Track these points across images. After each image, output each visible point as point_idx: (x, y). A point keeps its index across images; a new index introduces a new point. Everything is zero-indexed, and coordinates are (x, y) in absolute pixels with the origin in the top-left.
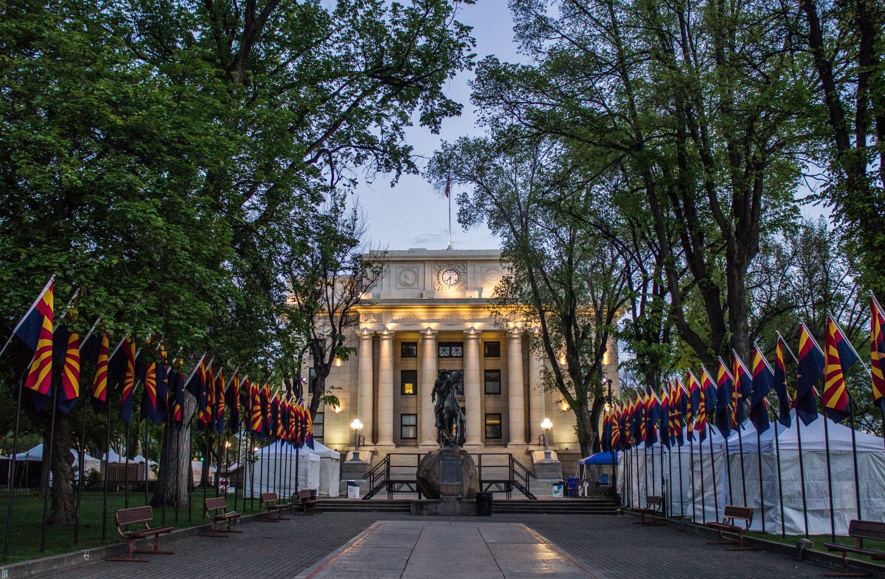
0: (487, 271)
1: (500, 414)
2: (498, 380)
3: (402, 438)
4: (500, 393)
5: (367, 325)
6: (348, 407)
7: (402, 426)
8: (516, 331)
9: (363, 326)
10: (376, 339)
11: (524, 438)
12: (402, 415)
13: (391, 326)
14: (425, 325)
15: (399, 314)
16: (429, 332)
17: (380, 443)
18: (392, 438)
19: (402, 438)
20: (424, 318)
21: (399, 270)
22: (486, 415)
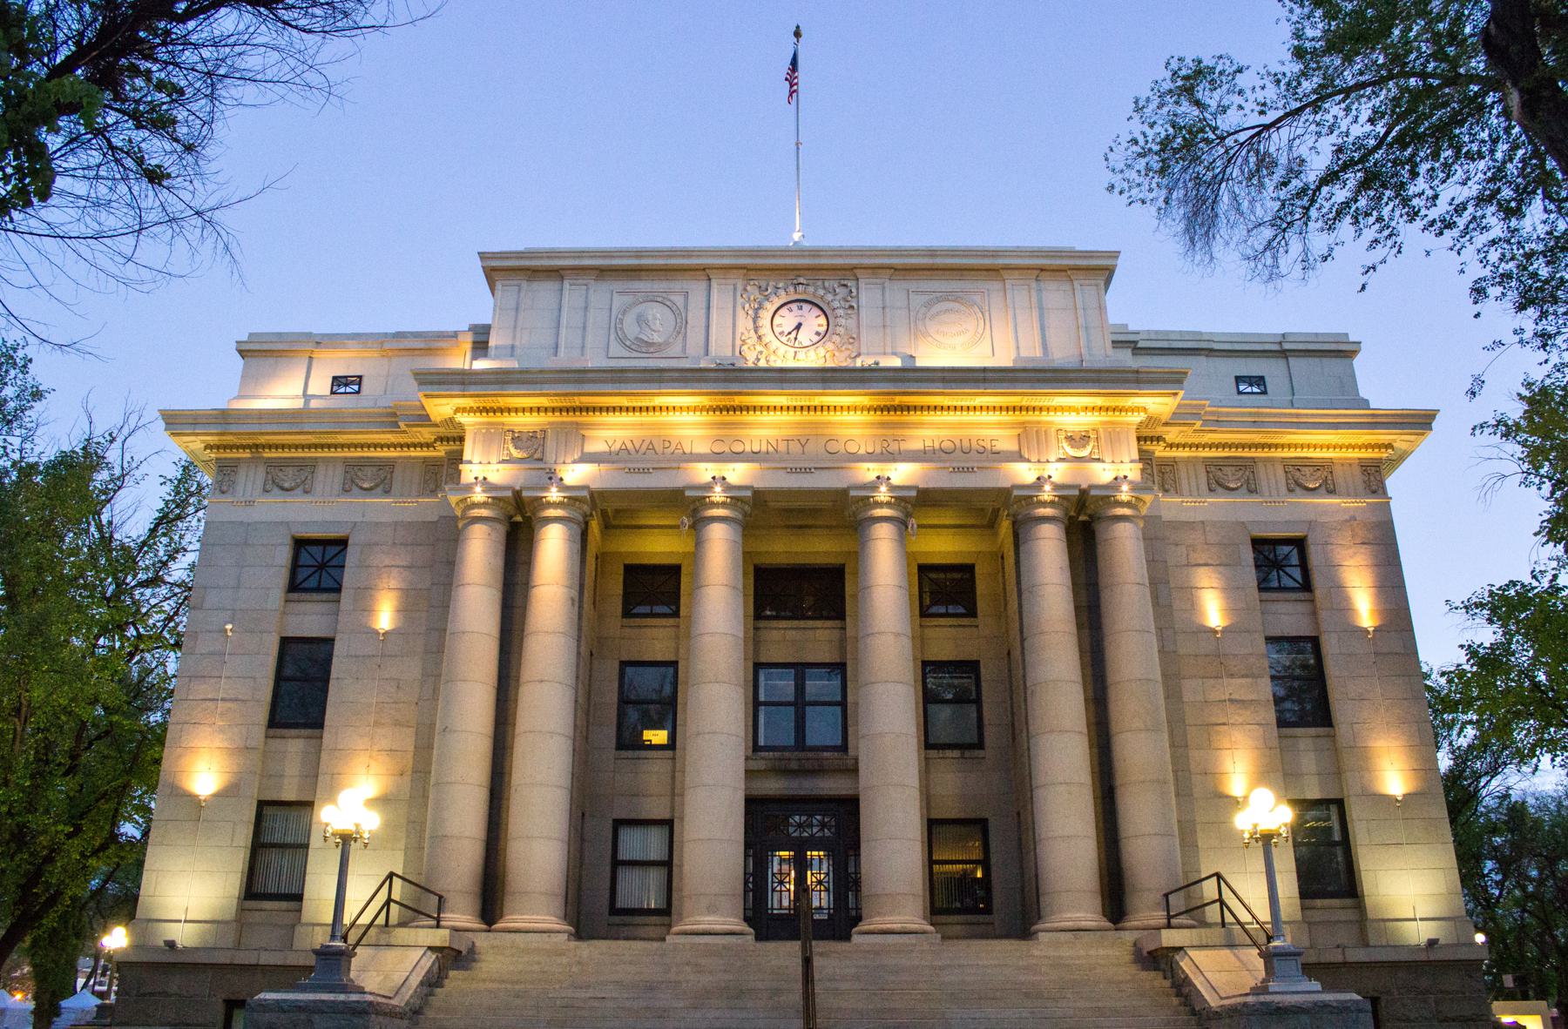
0: (929, 305)
1: (981, 825)
2: (970, 698)
3: (614, 910)
4: (980, 745)
5: (486, 468)
6: (407, 779)
7: (616, 863)
8: (1047, 494)
9: (469, 473)
10: (518, 526)
11: (1096, 902)
12: (619, 824)
13: (576, 474)
14: (704, 472)
15: (612, 431)
16: (718, 494)
17: (512, 920)
18: (558, 904)
19: (614, 910)
20: (702, 448)
21: (619, 301)
22: (925, 664)
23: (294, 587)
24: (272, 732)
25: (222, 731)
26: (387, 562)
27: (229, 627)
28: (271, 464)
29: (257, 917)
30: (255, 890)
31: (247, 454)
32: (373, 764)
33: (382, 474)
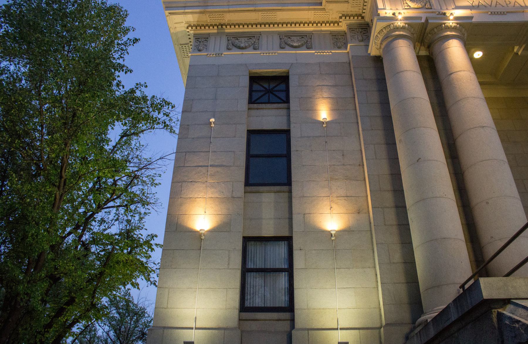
23: (251, 101)
24: (249, 189)
25: (212, 186)
26: (318, 84)
27: (212, 120)
28: (229, 36)
29: (254, 326)
30: (247, 304)
31: (215, 31)
32: (334, 206)
33: (304, 40)
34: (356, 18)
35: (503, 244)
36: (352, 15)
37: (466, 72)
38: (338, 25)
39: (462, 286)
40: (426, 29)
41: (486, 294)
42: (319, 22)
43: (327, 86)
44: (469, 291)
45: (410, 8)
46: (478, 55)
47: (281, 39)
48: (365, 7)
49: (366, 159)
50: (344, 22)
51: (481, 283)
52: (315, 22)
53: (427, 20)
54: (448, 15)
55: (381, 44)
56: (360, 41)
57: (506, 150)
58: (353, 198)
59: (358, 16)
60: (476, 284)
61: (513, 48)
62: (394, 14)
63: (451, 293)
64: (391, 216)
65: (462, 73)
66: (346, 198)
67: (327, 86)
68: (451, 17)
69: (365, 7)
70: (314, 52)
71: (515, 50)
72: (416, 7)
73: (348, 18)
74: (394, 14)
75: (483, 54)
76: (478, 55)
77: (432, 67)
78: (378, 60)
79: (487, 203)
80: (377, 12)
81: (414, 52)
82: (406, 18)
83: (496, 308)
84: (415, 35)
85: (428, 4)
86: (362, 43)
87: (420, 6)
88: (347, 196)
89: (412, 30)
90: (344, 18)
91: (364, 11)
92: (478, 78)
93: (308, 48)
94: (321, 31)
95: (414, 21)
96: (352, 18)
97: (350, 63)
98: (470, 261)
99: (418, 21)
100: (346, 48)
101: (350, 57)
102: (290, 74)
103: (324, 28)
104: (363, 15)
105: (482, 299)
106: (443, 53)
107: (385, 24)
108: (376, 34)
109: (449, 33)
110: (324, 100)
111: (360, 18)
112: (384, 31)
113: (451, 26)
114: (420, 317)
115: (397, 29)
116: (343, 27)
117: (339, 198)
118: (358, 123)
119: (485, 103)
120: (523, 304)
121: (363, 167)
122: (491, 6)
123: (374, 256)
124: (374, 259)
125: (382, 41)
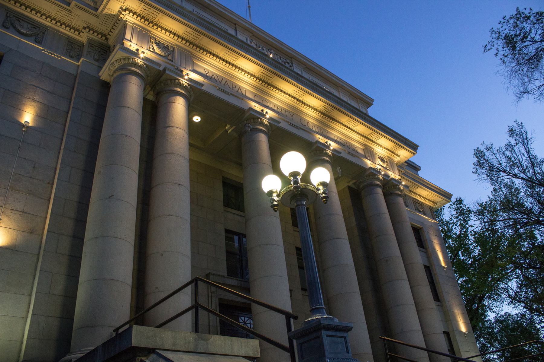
34: (100, 36)
35: (163, 296)
36: (97, 31)
37: (181, 130)
38: (79, 34)
39: (116, 330)
40: (161, 77)
41: (135, 342)
42: (59, 21)
43: (43, 89)
44: (121, 335)
45: (154, 52)
46: (197, 119)
47: (7, 17)
48: (112, 30)
49: (58, 179)
50: (86, 34)
51: (133, 330)
52: (55, 19)
53: (164, 70)
54: (184, 73)
55: (114, 72)
56: (95, 60)
57: (192, 210)
58: (30, 216)
59: (103, 35)
60: (130, 330)
61: (226, 126)
62: (137, 50)
63: (104, 334)
64: (65, 244)
65: (177, 130)
66: (21, 213)
67: (43, 89)
68: (186, 77)
69: (112, 30)
70: (42, 48)
71: (227, 128)
72: (160, 53)
73: (91, 32)
74: (137, 50)
75: (193, 117)
76: (197, 119)
77: (154, 114)
78: (106, 86)
79: (162, 255)
80: (123, 40)
81: (142, 93)
82: (146, 59)
83: (140, 356)
84: (149, 78)
85: (171, 56)
86: (97, 64)
87: (163, 54)
88: (23, 212)
89: (149, 72)
90: (87, 30)
91: (110, 33)
92: (189, 139)
93: (36, 42)
94: (58, 31)
95: (151, 65)
96: (95, 34)
97: (76, 77)
98: (131, 307)
99: (157, 67)
100: (78, 61)
101: (79, 71)
102: (4, 58)
103: (62, 29)
104: (108, 36)
105: (130, 346)
106: (168, 107)
107: (125, 55)
108: (113, 61)
109: (179, 90)
110: (33, 103)
111: (104, 38)
112: (122, 61)
113: (183, 84)
114: (65, 356)
115: (135, 65)
116: (83, 38)
117: (13, 212)
118: (62, 140)
119: (188, 165)
120: (164, 355)
121: (52, 187)
122: (221, 83)
123: (33, 283)
124: (32, 287)
125: (117, 70)
